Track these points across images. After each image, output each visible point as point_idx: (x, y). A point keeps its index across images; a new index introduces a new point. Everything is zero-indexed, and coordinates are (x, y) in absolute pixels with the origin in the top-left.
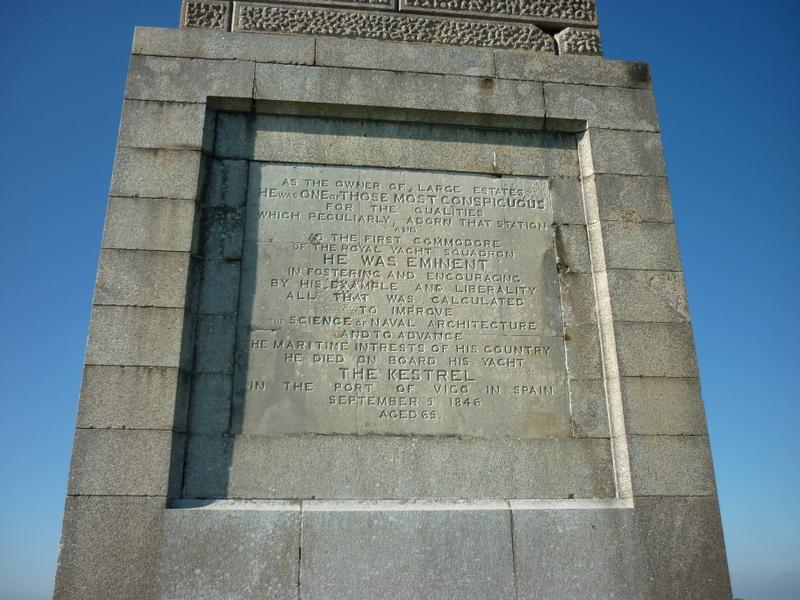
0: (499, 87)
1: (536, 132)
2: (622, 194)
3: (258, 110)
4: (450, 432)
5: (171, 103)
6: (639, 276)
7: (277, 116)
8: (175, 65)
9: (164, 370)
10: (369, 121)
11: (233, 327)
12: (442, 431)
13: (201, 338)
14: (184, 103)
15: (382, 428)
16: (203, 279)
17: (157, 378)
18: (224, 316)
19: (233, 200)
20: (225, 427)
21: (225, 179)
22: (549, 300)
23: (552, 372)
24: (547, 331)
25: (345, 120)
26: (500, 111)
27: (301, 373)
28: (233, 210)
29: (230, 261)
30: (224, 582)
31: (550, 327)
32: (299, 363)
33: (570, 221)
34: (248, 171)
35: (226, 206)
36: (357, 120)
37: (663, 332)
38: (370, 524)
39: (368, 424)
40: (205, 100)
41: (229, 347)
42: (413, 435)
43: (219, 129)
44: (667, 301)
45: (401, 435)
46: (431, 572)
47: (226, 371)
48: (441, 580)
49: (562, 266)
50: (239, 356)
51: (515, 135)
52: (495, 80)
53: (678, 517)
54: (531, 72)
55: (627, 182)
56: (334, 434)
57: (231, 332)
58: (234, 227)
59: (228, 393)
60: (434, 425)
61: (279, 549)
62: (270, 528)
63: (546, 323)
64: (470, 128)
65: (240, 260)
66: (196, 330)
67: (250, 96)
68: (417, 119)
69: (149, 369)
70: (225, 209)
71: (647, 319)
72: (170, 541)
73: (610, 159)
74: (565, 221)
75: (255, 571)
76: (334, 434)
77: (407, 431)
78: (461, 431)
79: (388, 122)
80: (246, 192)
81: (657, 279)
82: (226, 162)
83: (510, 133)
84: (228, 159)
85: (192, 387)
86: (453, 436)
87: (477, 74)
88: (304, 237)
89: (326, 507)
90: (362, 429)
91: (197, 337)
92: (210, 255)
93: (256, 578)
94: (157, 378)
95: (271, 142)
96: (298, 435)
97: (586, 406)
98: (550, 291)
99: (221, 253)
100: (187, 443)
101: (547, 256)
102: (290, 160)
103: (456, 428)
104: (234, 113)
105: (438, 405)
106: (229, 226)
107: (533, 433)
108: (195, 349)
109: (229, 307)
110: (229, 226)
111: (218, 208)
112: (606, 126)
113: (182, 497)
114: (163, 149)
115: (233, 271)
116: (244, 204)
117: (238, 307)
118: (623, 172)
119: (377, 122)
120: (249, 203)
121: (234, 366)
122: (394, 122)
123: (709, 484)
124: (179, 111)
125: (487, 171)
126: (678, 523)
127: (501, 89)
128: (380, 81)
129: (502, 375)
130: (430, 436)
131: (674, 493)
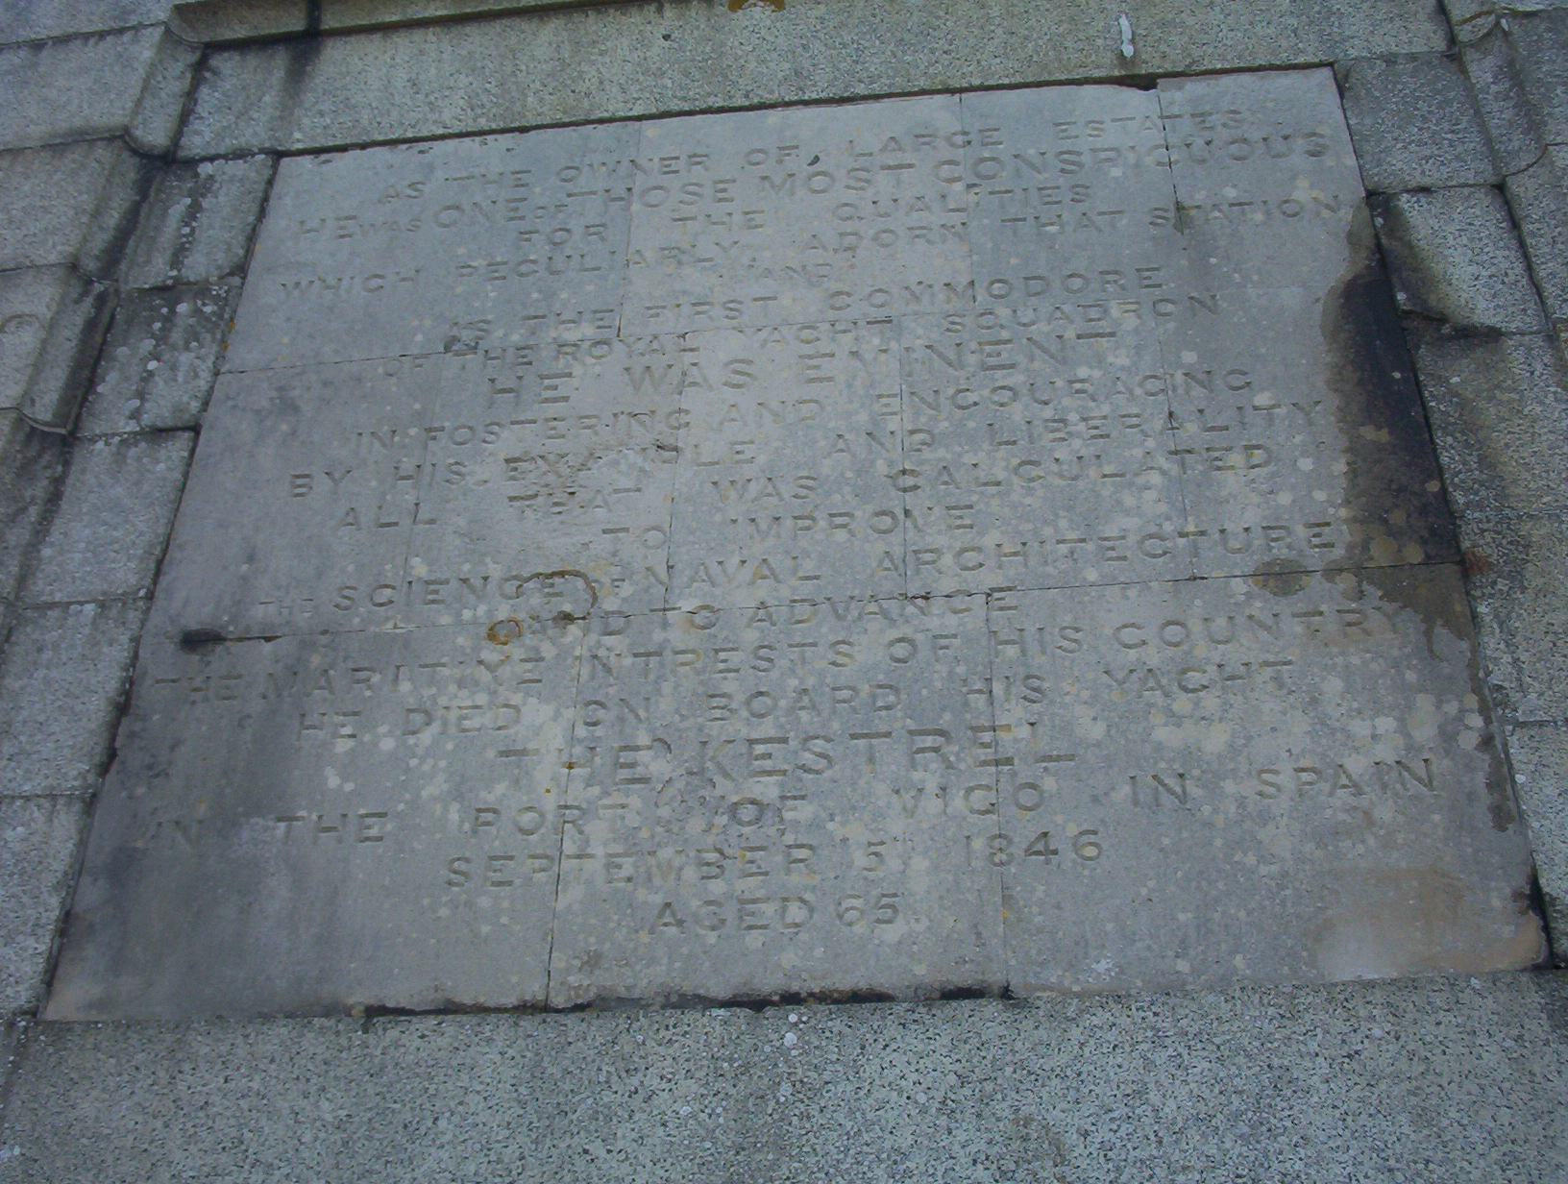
7: (387, 29)
11: (125, 639)
12: (921, 971)
18: (102, 605)
27: (345, 779)
31: (1393, 533)
32: (343, 746)
33: (1432, 176)
41: (96, 708)
50: (132, 735)
58: (193, 335)
65: (195, 429)
74: (1419, 180)
76: (450, 1009)
84: (212, 159)
90: (575, 982)
99: (135, 415)
102: (410, 135)
103: (612, 747)
110: (177, 336)
114: (1006, 994)
116: (241, 269)
125: (1097, 74)
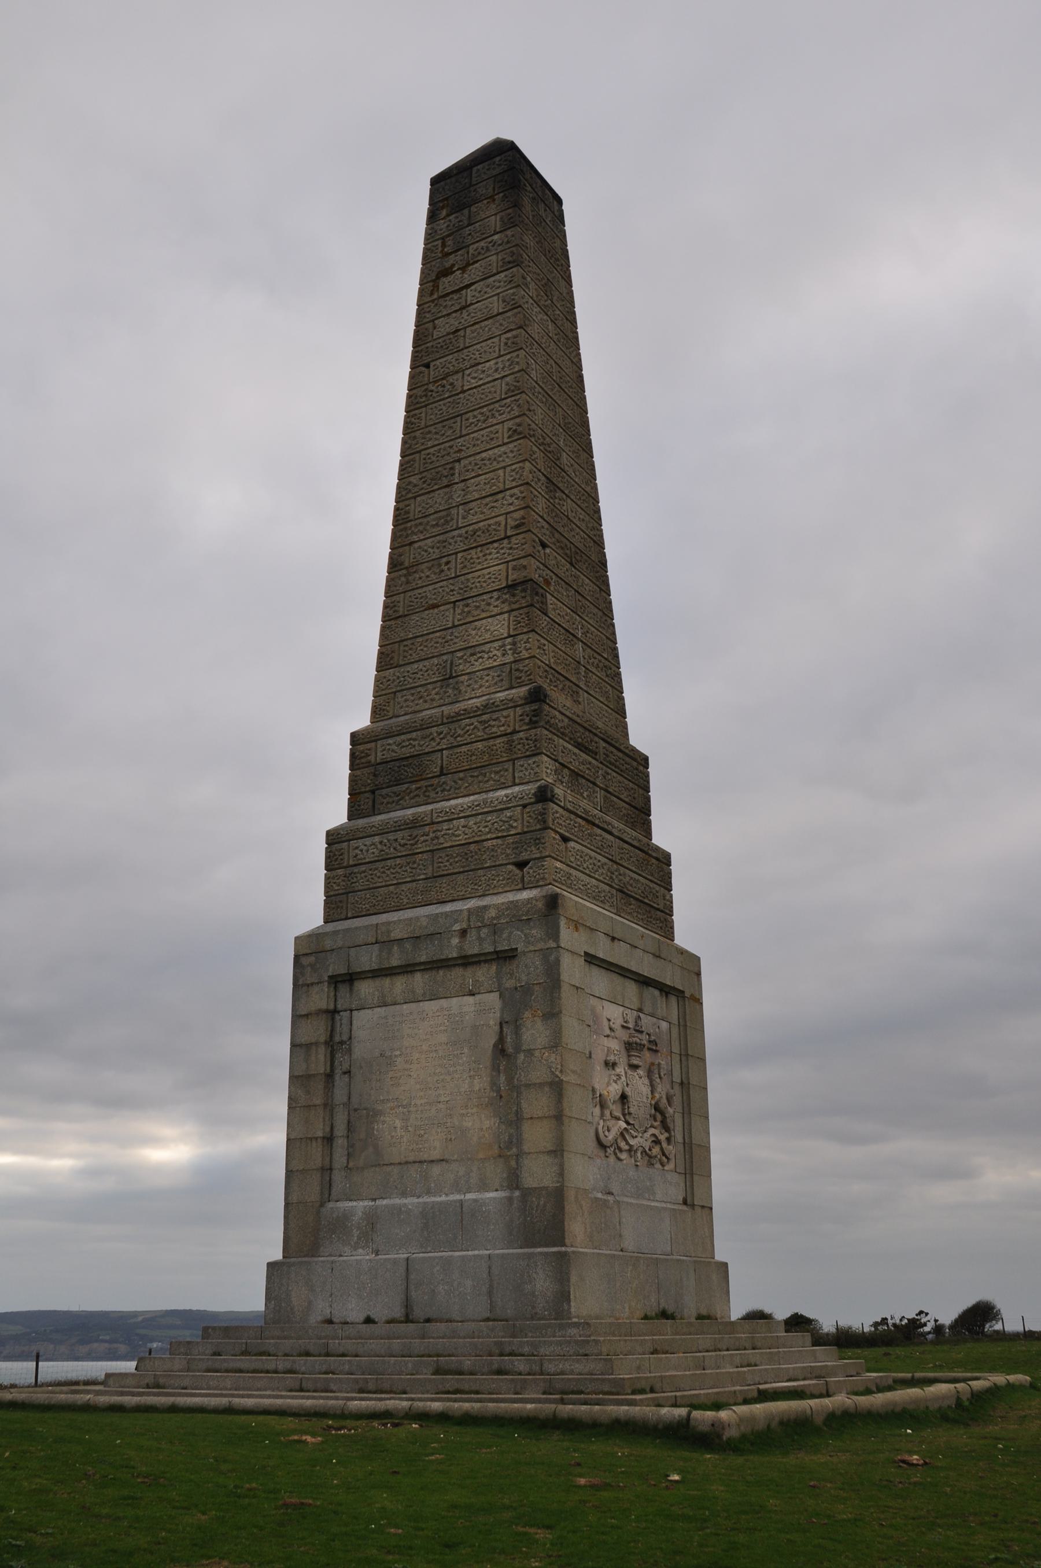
0: (471, 934)
1: (494, 959)
2: (533, 998)
3: (354, 978)
4: (442, 1158)
5: (312, 984)
6: (537, 1053)
8: (312, 959)
9: (316, 1139)
10: (407, 972)
13: (335, 1119)
14: (318, 983)
15: (411, 1159)
16: (334, 1085)
17: (314, 1142)
19: (345, 1038)
20: (345, 1165)
21: (341, 1024)
22: (494, 1074)
23: (493, 1119)
24: (491, 1094)
25: (395, 974)
26: (470, 953)
28: (345, 1043)
29: (345, 1073)
30: (343, 1240)
31: (493, 1091)
32: (376, 1127)
34: (351, 1017)
35: (342, 1041)
36: (401, 973)
37: (547, 1089)
38: (401, 1209)
39: (405, 1157)
40: (326, 979)
42: (425, 1161)
43: (337, 993)
44: (550, 1068)
45: (420, 1162)
46: (425, 1233)
47: (345, 1135)
48: (430, 1237)
49: (503, 1051)
51: (482, 964)
52: (469, 930)
53: (542, 1199)
54: (489, 918)
55: (536, 988)
56: (391, 1164)
57: (346, 1113)
59: (346, 1146)
60: (436, 1155)
61: (364, 1224)
62: (360, 1214)
63: (492, 1088)
64: (458, 965)
65: (350, 1072)
66: (332, 1115)
67: (347, 972)
68: (430, 966)
69: (311, 1139)
70: (342, 1043)
71: (538, 1081)
72: (323, 1223)
73: (529, 974)
75: (356, 1235)
76: (391, 1164)
77: (423, 1159)
78: (446, 1157)
79: (417, 970)
80: (351, 1031)
81: (547, 1054)
82: (341, 1013)
83: (480, 964)
85: (332, 1145)
86: (443, 1160)
87: (458, 928)
88: (377, 1054)
89: (385, 1202)
91: (332, 1118)
92: (336, 1071)
93: (356, 1238)
94: (314, 1142)
95: (497, 911)
96: (376, 1166)
97: (507, 1138)
98: (495, 1068)
99: (341, 1069)
100: (331, 1174)
101: (495, 1046)
104: (343, 981)
105: (437, 1144)
106: (344, 1053)
107: (481, 1156)
108: (332, 1124)
109: (345, 1099)
111: (339, 1043)
112: (528, 950)
113: (329, 1201)
115: (346, 1078)
116: (350, 1038)
117: (349, 1098)
118: (535, 982)
119: (411, 972)
120: (353, 1037)
121: (348, 1132)
122: (419, 970)
123: (561, 1180)
124: (316, 989)
126: (542, 1203)
127: (472, 935)
128: (330, 1000)
129: (468, 1123)
130: (432, 1161)
131: (541, 1186)
